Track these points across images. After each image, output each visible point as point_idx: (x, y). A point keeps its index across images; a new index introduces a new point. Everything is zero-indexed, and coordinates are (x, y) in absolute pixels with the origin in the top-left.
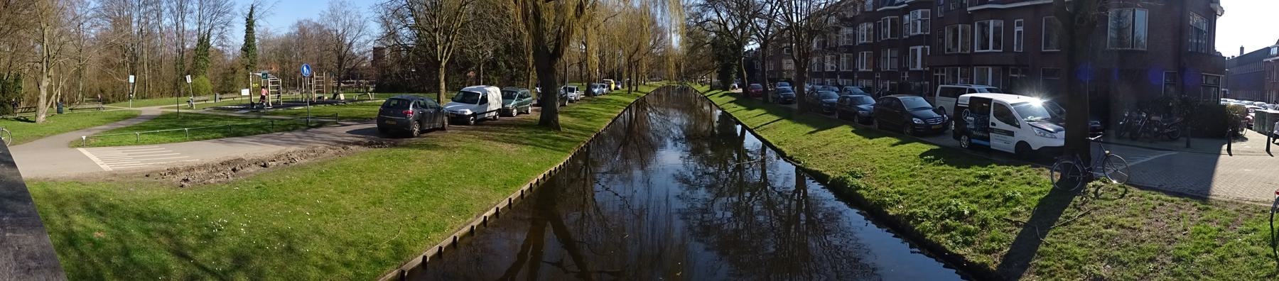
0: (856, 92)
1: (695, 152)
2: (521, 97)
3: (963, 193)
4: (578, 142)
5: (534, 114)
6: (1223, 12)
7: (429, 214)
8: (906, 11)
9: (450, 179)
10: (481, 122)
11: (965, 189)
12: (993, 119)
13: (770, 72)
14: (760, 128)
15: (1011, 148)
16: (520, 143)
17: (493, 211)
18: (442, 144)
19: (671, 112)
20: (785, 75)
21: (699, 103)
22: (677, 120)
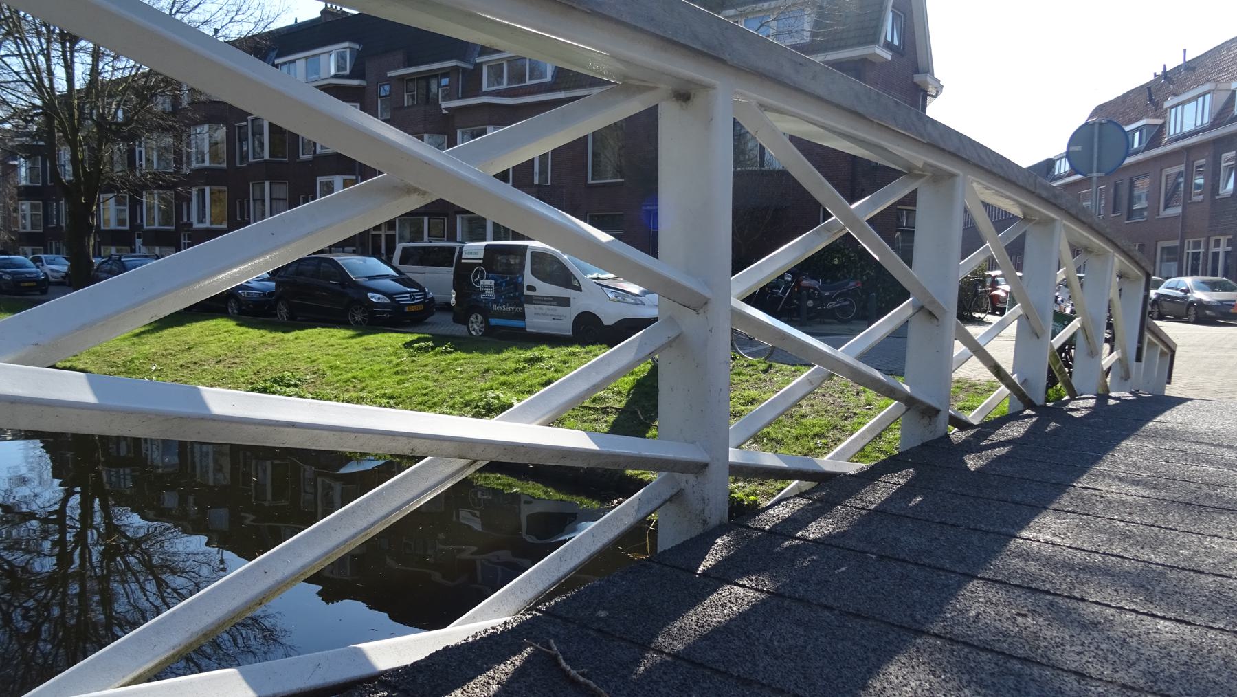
3: (504, 384)
6: (939, 88)
11: (503, 378)
12: (529, 279)
15: (564, 326)
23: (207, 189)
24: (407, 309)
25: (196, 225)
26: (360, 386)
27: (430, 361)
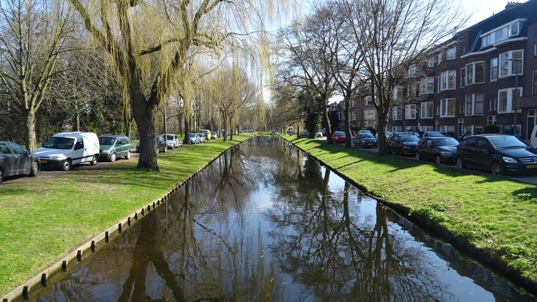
0: (436, 135)
1: (285, 193)
2: (120, 143)
4: (177, 181)
5: (133, 159)
7: (11, 256)
8: (494, 55)
9: (37, 220)
10: (75, 166)
13: (353, 122)
14: (342, 171)
16: (119, 183)
17: (88, 245)
18: (29, 188)
19: (263, 159)
20: (367, 124)
21: (287, 151)
22: (269, 165)
23: (447, 100)
24: (528, 167)
25: (442, 116)
26: (476, 217)
27: (525, 207)
